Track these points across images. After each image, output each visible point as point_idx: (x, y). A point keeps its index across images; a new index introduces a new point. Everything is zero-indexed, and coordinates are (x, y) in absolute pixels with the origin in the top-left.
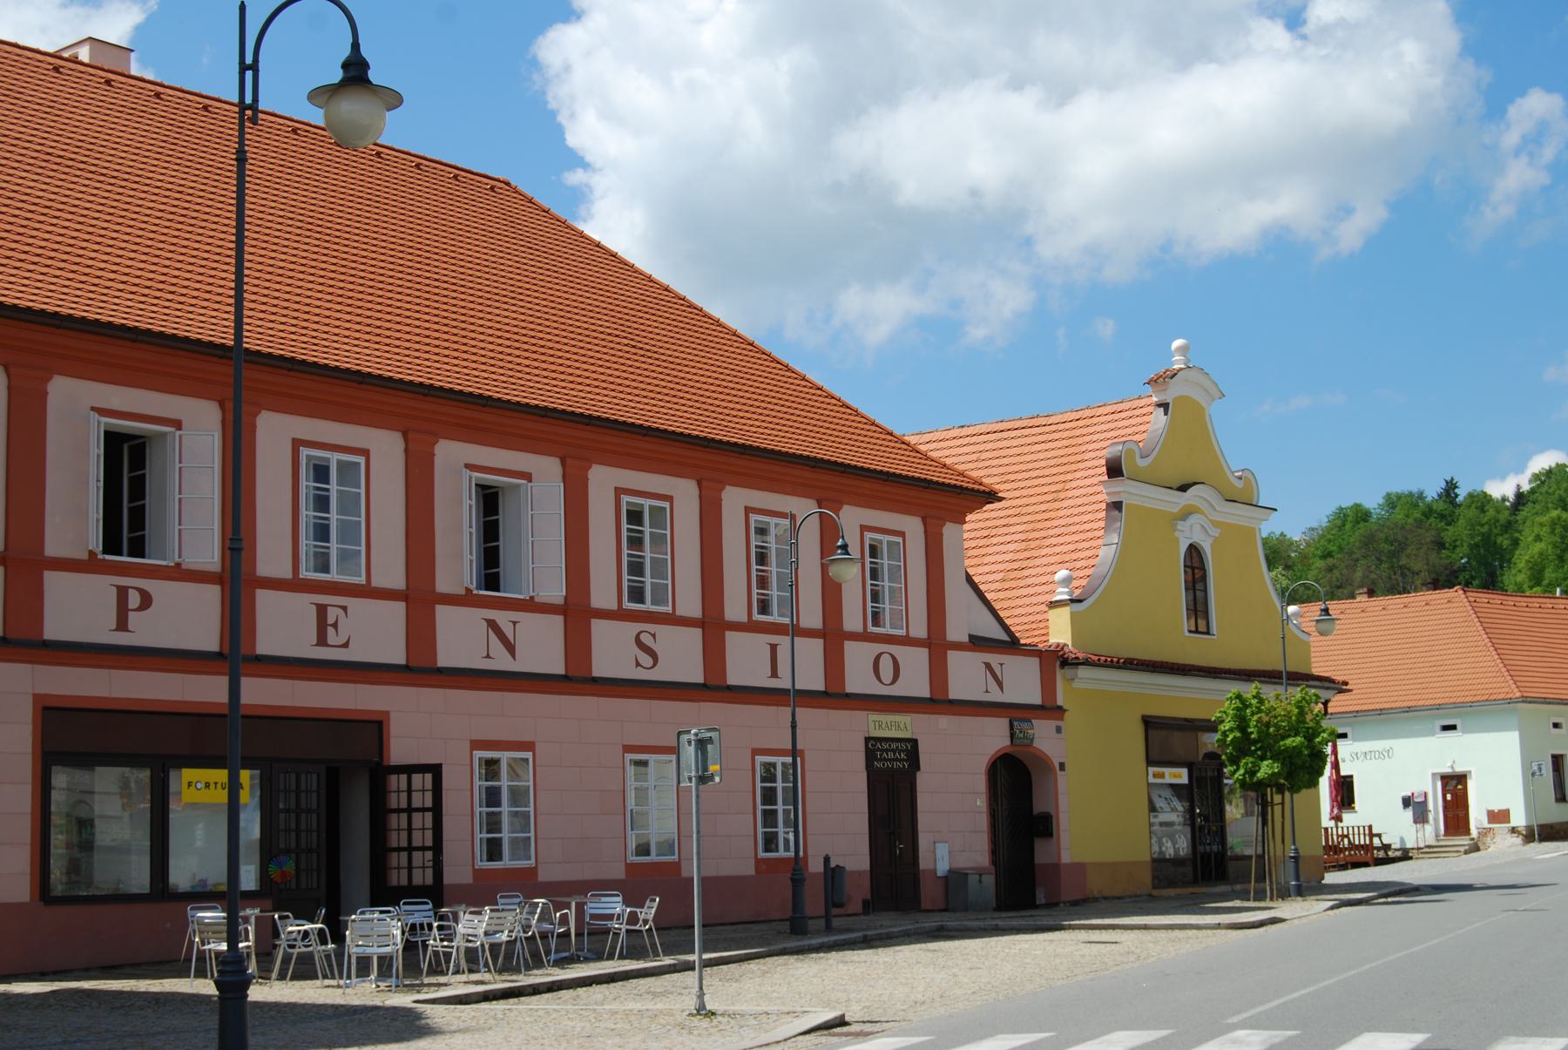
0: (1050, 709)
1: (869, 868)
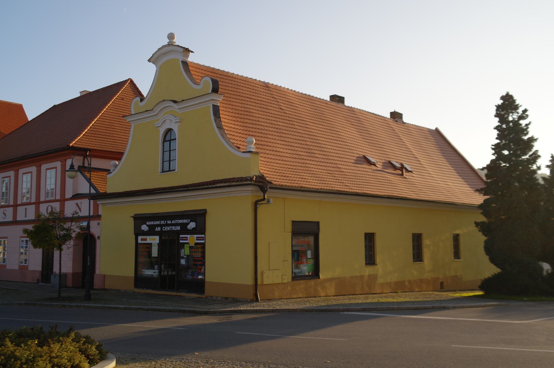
0: (97, 217)
1: (39, 268)
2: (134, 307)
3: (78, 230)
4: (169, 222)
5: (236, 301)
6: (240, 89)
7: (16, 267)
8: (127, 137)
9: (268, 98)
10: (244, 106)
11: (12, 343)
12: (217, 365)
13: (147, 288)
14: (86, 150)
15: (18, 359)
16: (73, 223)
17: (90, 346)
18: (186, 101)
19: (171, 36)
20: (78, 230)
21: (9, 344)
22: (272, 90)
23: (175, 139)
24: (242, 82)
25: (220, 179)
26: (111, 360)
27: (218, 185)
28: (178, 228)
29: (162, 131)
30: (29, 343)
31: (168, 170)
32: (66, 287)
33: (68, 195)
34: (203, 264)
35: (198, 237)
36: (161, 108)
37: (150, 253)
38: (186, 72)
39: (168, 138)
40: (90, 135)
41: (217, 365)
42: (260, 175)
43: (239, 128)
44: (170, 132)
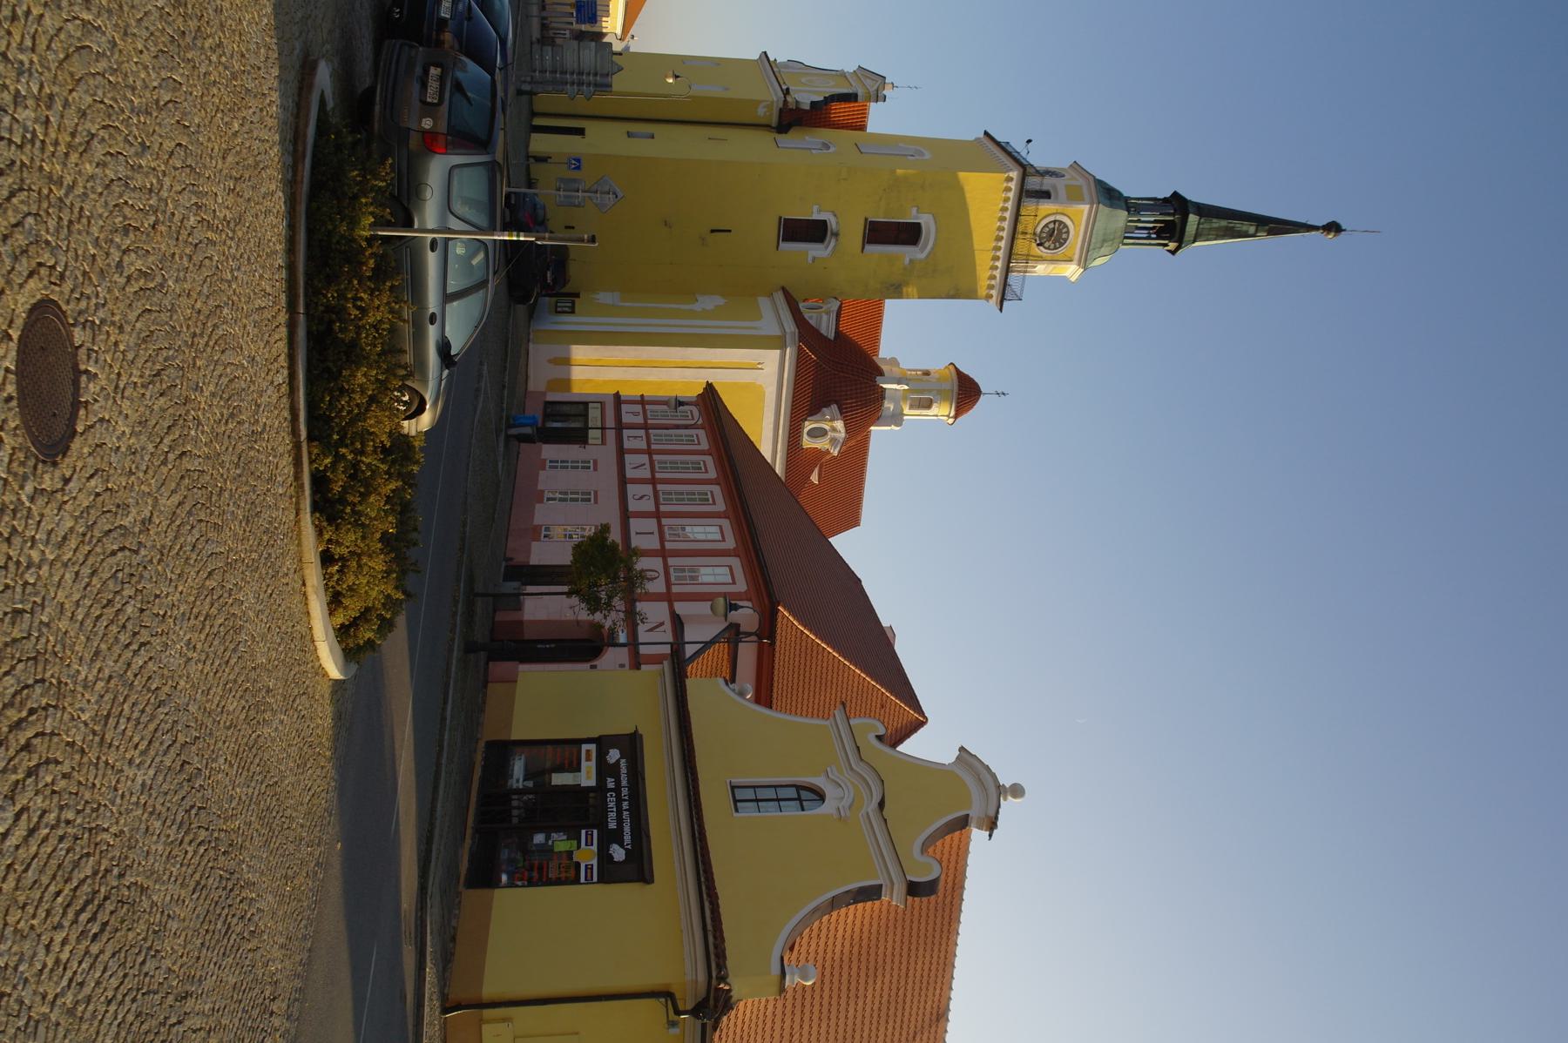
0: (636, 662)
1: (534, 561)
2: (446, 737)
3: (608, 624)
4: (625, 805)
5: (446, 960)
6: (925, 950)
7: (537, 520)
8: (804, 713)
9: (913, 1019)
10: (888, 960)
11: (393, 491)
12: (310, 883)
13: (484, 768)
14: (772, 635)
15: (362, 500)
16: (622, 615)
17: (375, 627)
18: (884, 827)
19: (1017, 791)
20: (608, 624)
21: (392, 486)
22: (933, 1030)
23: (803, 810)
24: (942, 955)
25: (722, 910)
26: (344, 670)
27: (707, 904)
28: (612, 825)
29: (819, 782)
30: (390, 518)
31: (737, 798)
32: (495, 611)
33: (681, 608)
34: (531, 883)
35: (592, 869)
36: (865, 776)
37: (560, 769)
38: (947, 824)
39: (804, 794)
40: (804, 644)
41: (310, 883)
42: (733, 1000)
43: (838, 950)
44: (816, 797)
